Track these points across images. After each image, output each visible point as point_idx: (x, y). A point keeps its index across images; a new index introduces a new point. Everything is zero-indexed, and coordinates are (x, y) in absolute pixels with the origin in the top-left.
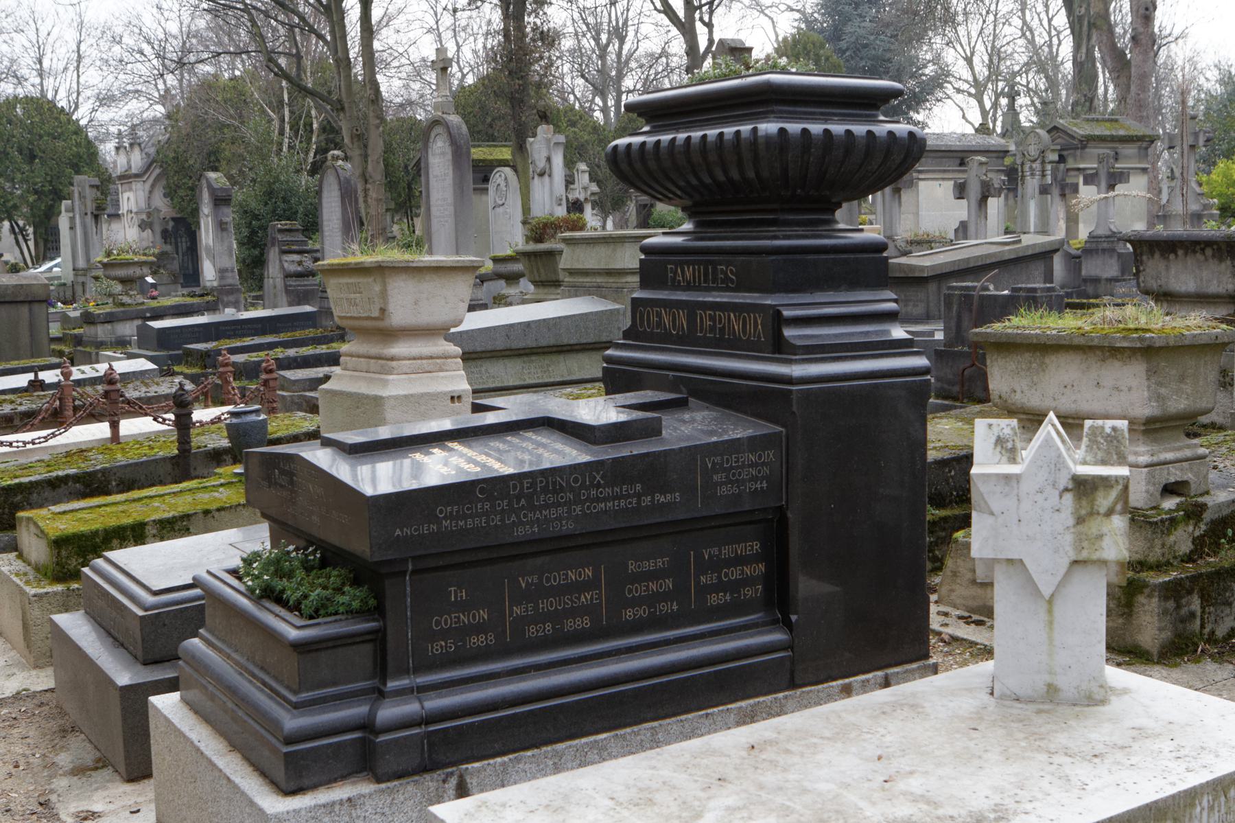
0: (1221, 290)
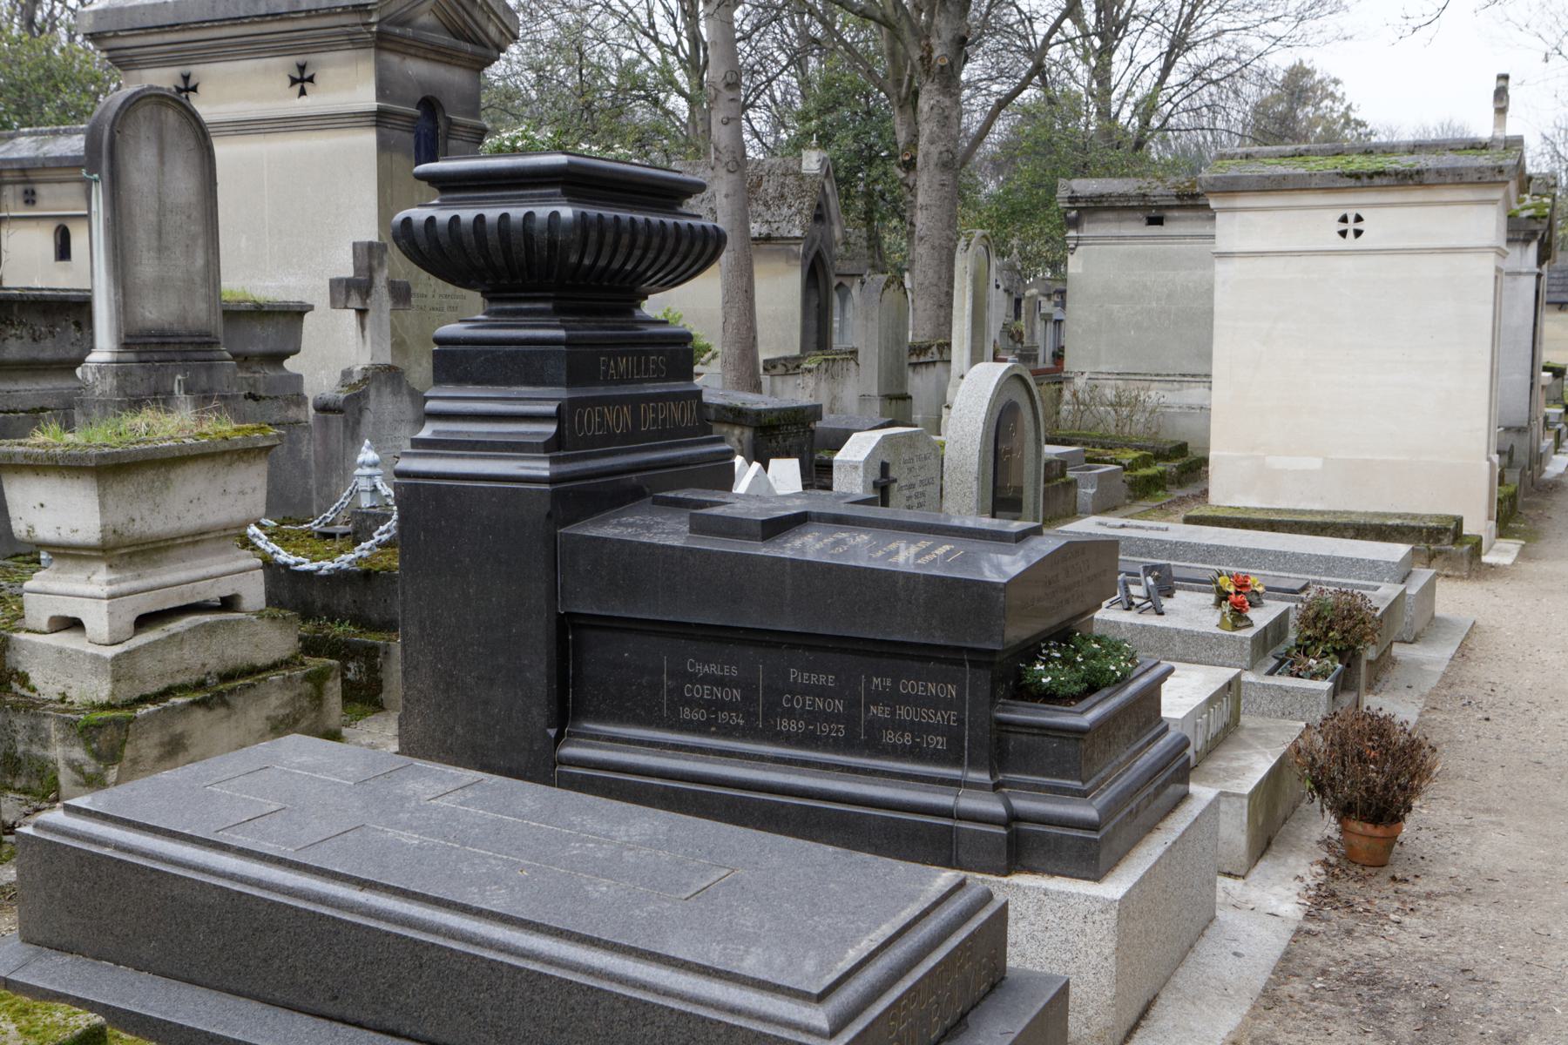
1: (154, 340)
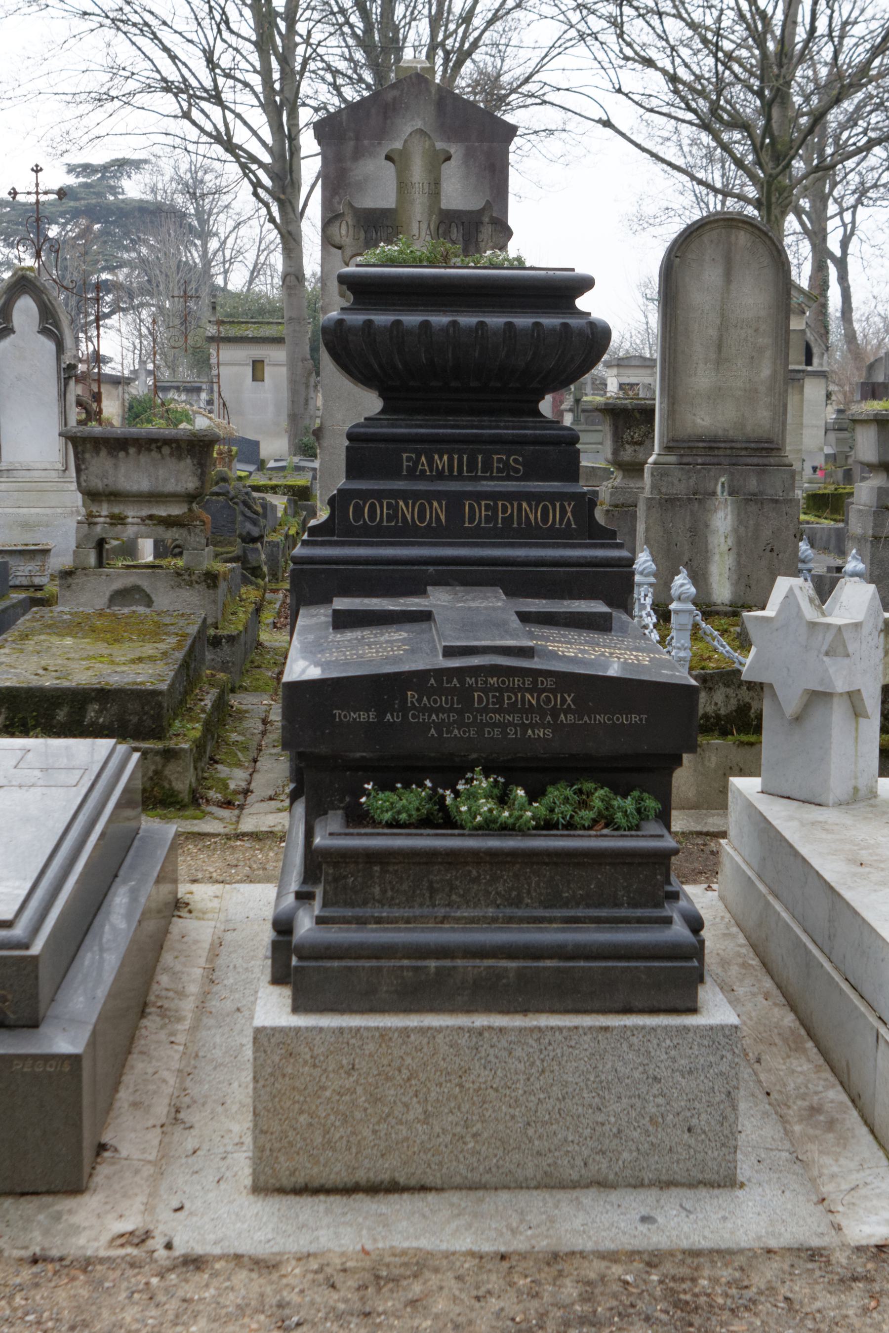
0: (180, 488)
1: (701, 445)
